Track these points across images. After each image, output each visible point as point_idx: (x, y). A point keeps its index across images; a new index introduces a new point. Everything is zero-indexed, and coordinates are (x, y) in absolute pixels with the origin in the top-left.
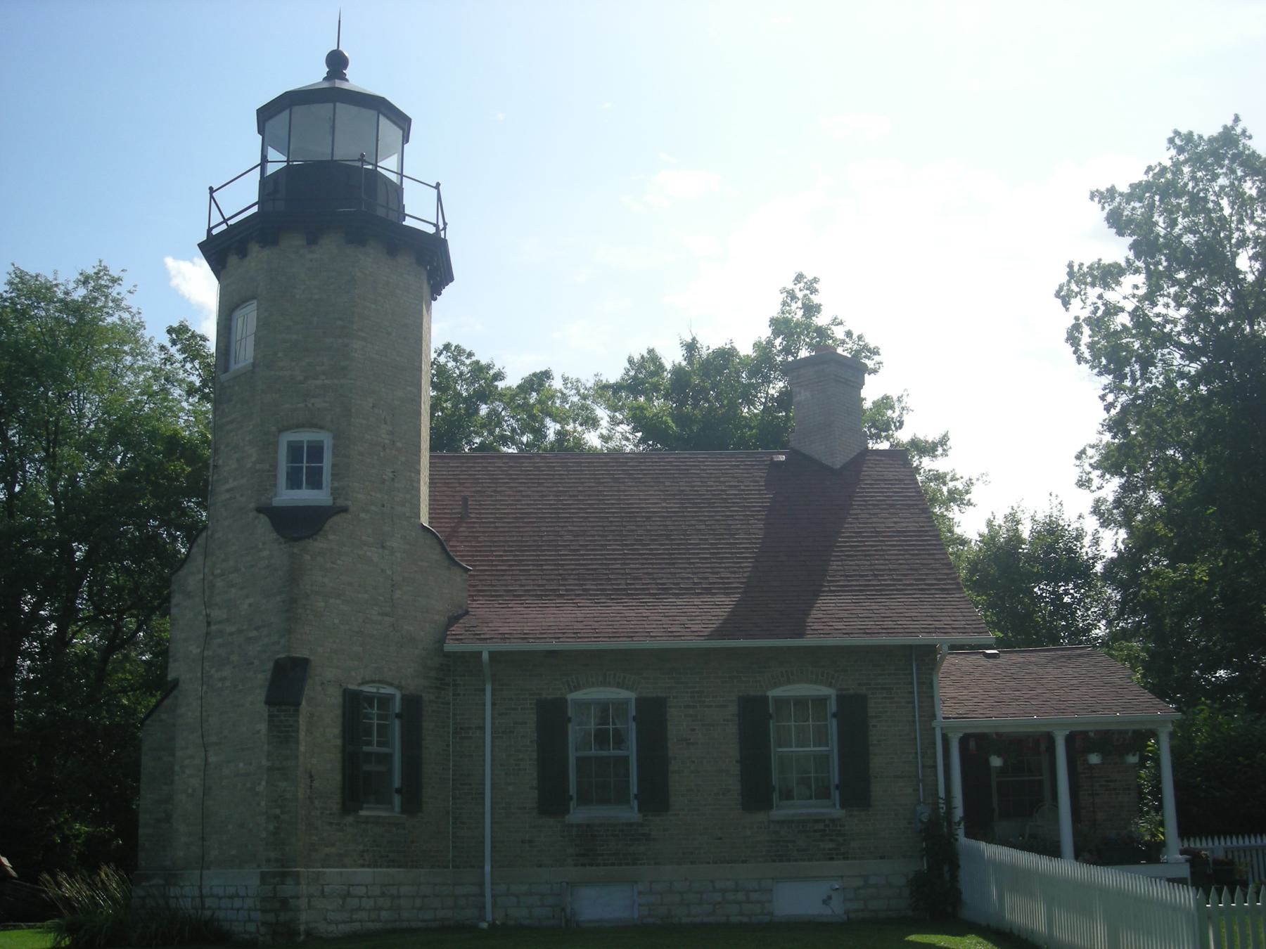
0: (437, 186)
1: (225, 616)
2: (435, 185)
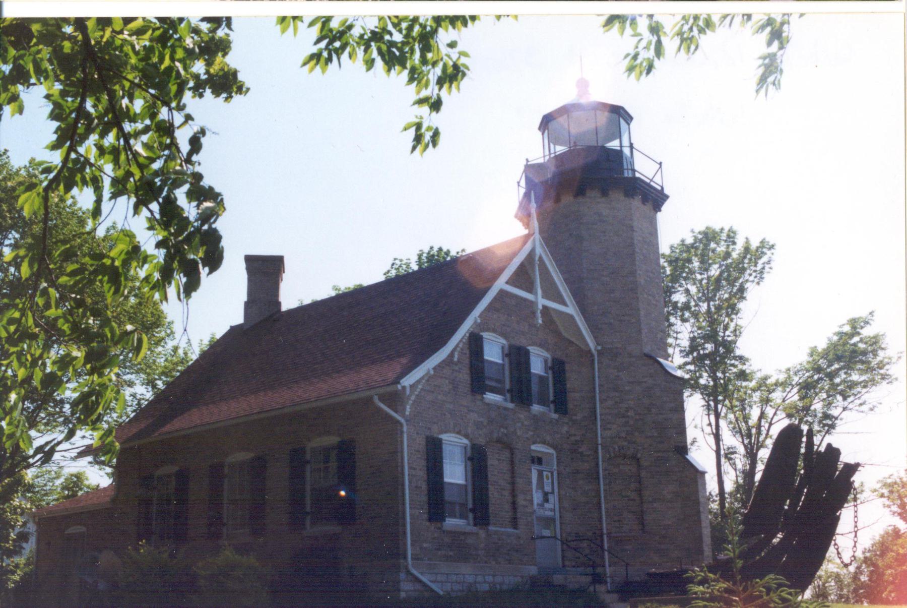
0: (660, 164)
2: (659, 162)
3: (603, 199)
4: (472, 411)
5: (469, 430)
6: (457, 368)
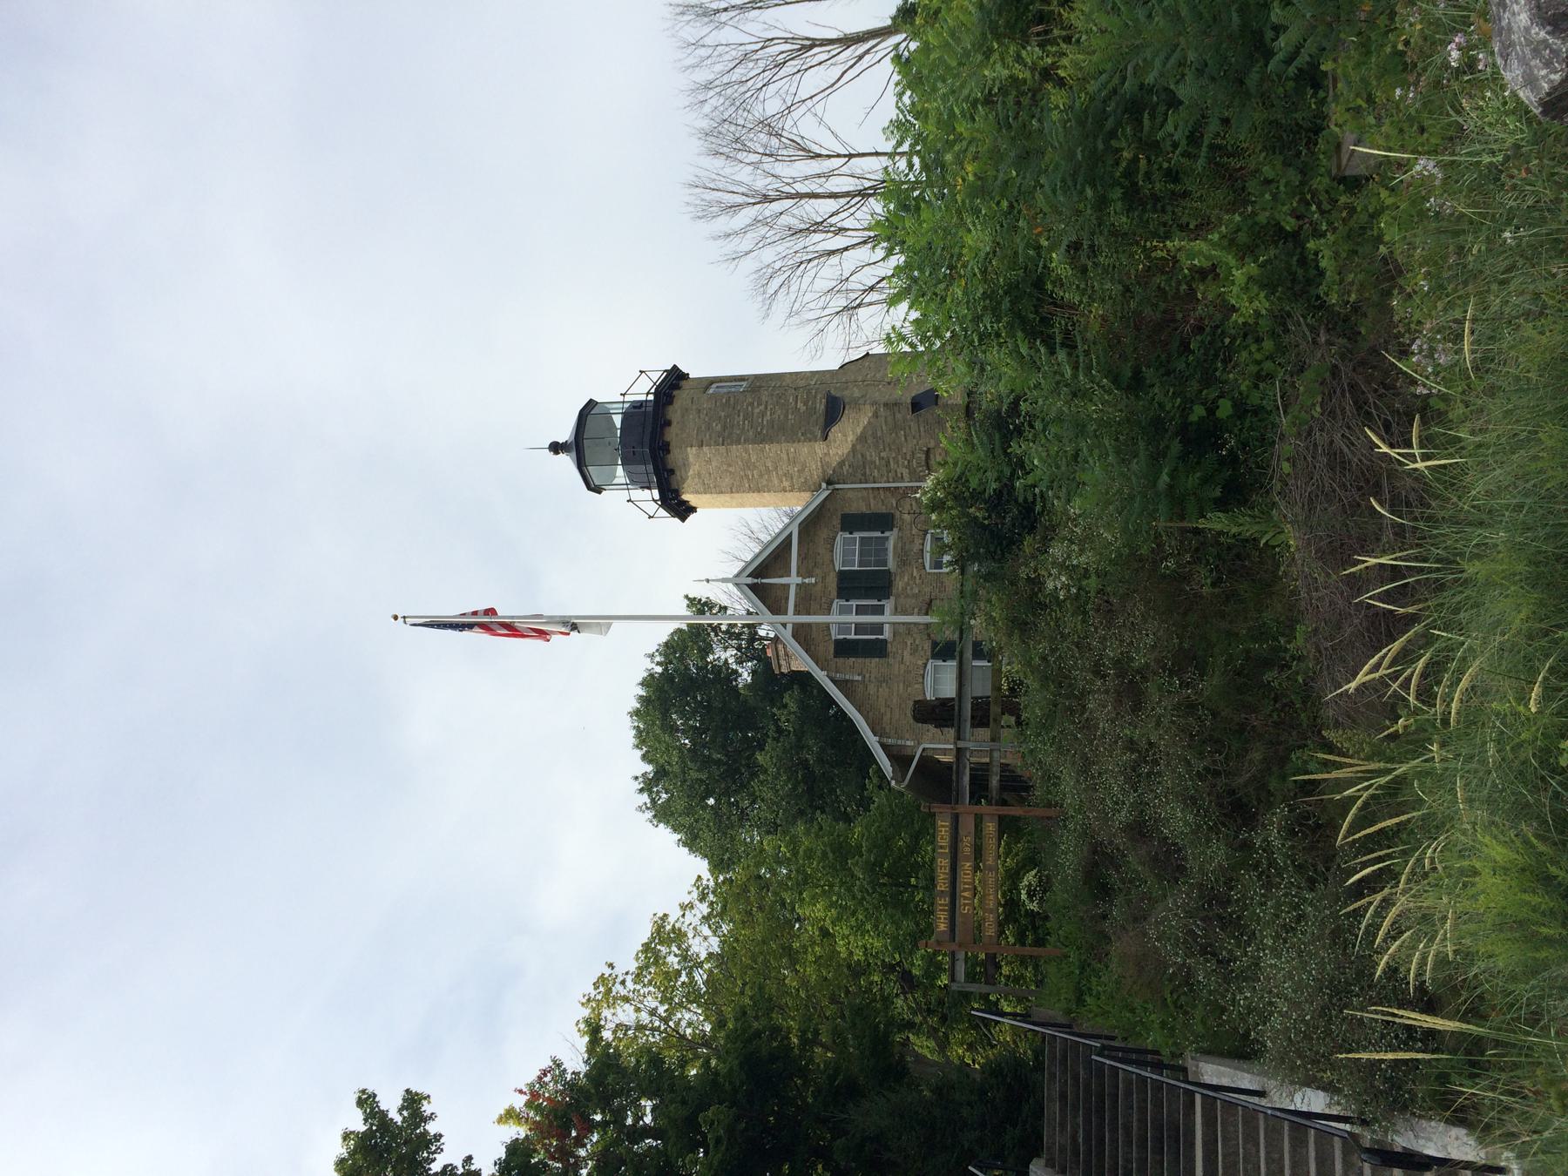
3: (678, 473)
5: (920, 663)
6: (867, 676)
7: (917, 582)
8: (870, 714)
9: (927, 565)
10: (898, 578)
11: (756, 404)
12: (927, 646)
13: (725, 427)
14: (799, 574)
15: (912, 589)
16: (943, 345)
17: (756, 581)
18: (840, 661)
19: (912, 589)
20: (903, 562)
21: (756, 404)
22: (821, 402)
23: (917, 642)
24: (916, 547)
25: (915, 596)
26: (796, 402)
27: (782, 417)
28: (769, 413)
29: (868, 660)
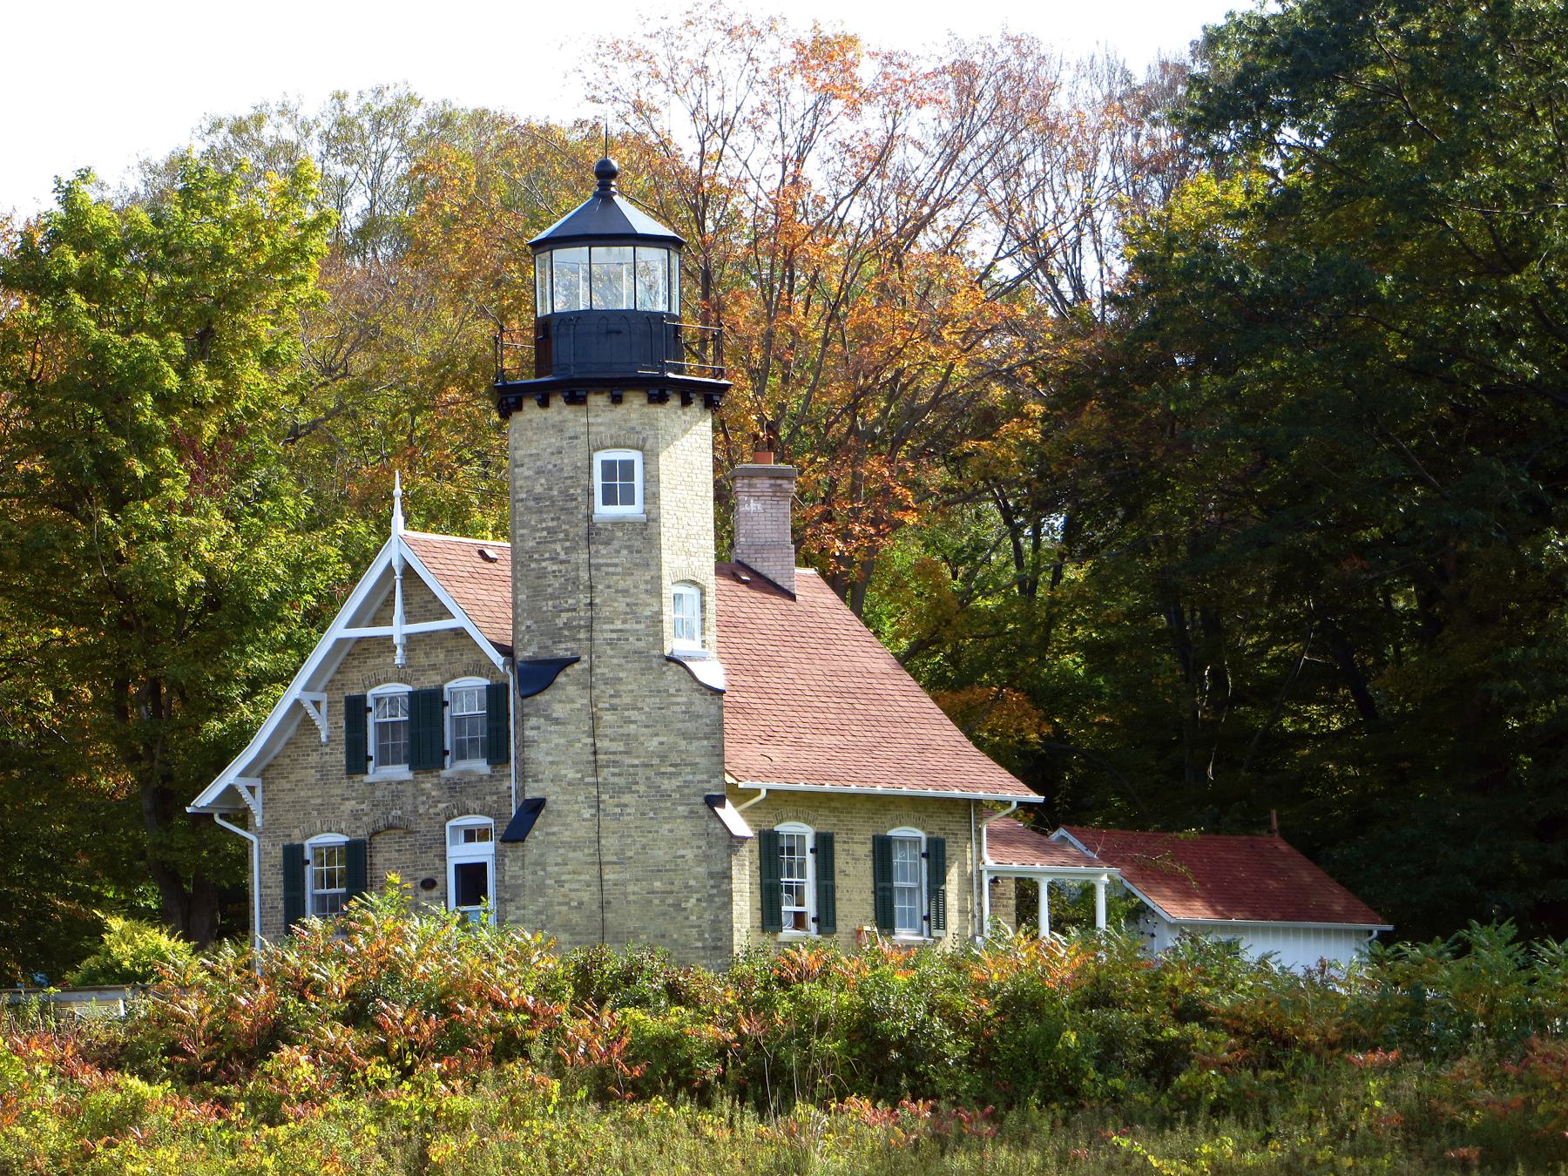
1: (622, 749)
4: (348, 799)
6: (328, 750)
7: (431, 811)
8: (287, 761)
9: (314, 840)
10: (435, 780)
11: (568, 544)
12: (362, 834)
13: (537, 499)
14: (409, 637)
15: (423, 803)
16: (113, 899)
17: (398, 572)
18: (342, 707)
19: (423, 803)
20: (454, 787)
21: (568, 544)
22: (566, 650)
23: (365, 819)
24: (470, 804)
25: (415, 811)
26: (568, 610)
27: (550, 590)
28: (555, 568)
29: (342, 748)
